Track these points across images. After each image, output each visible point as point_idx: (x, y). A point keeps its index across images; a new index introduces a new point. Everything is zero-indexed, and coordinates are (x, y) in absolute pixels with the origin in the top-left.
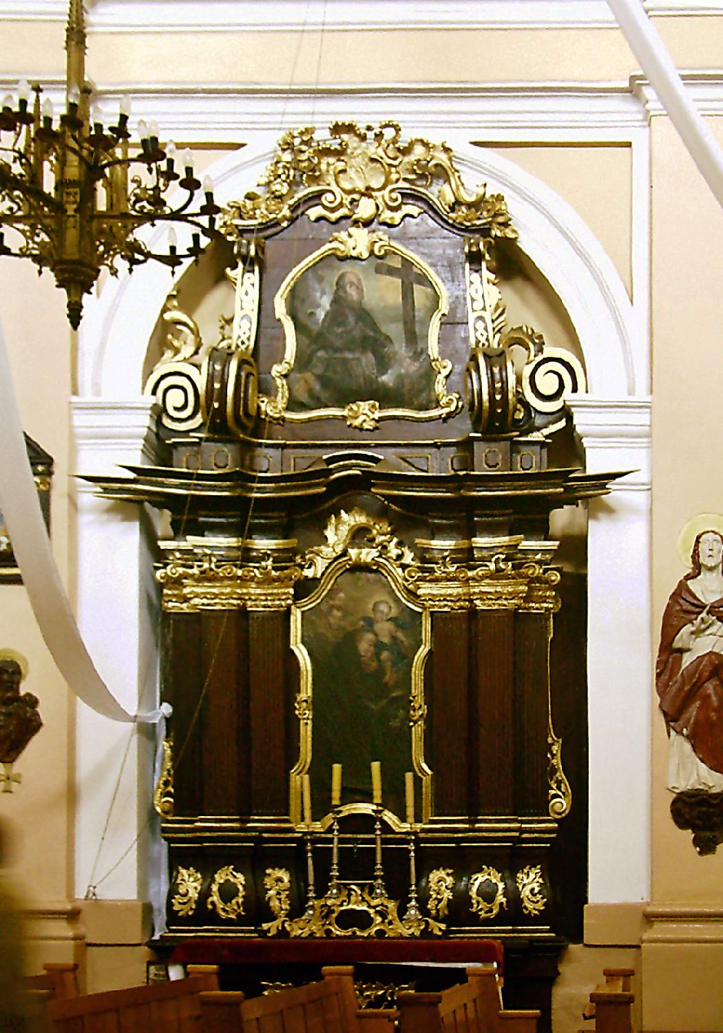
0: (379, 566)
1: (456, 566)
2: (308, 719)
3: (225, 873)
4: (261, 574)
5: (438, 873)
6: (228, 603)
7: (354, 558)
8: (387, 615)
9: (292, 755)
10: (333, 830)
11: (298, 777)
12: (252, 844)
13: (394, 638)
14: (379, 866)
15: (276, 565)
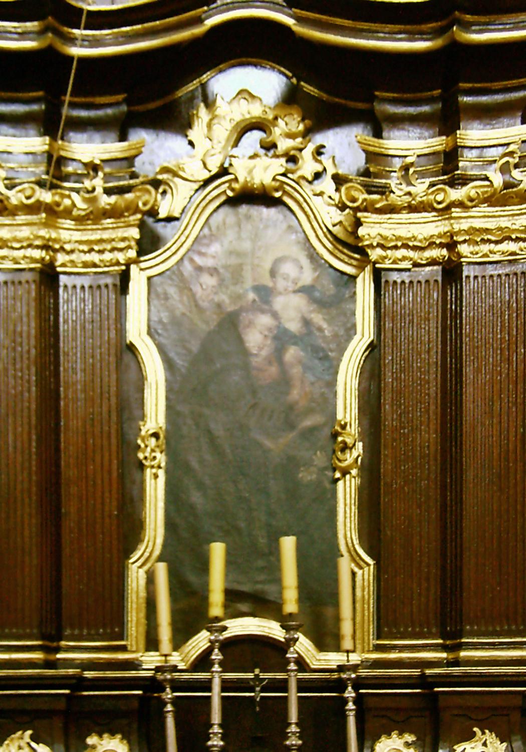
0: (285, 192)
1: (427, 181)
2: (159, 467)
3: (16, 744)
4: (86, 200)
5: (389, 742)
6: (25, 257)
7: (241, 180)
8: (295, 282)
9: (131, 531)
10: (212, 664)
11: (140, 570)
12: (140, 692)
13: (306, 322)
14: (293, 728)
15: (111, 185)
